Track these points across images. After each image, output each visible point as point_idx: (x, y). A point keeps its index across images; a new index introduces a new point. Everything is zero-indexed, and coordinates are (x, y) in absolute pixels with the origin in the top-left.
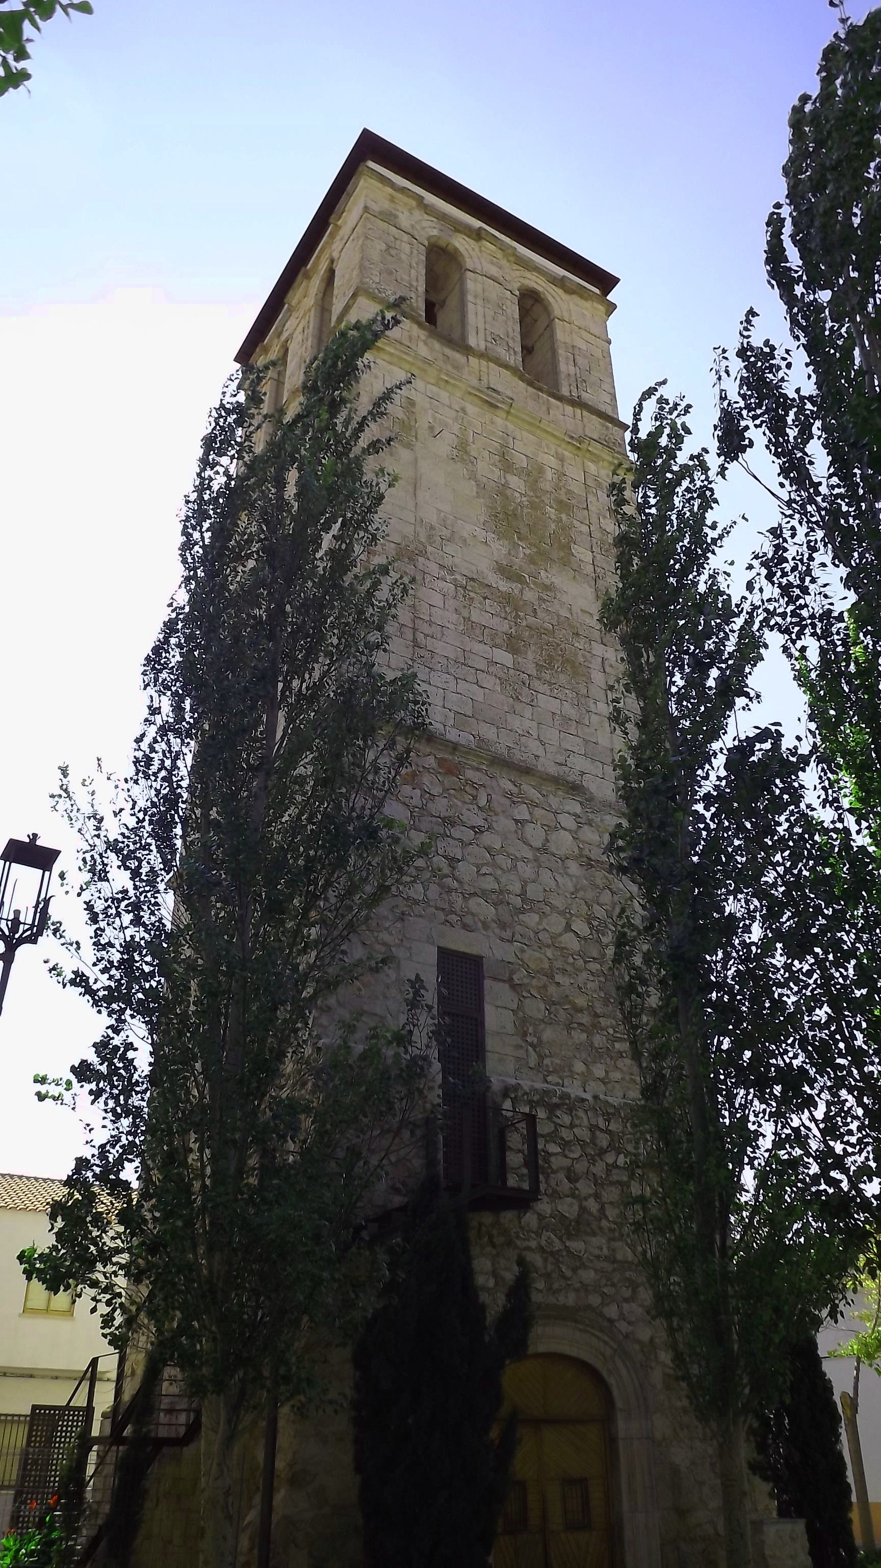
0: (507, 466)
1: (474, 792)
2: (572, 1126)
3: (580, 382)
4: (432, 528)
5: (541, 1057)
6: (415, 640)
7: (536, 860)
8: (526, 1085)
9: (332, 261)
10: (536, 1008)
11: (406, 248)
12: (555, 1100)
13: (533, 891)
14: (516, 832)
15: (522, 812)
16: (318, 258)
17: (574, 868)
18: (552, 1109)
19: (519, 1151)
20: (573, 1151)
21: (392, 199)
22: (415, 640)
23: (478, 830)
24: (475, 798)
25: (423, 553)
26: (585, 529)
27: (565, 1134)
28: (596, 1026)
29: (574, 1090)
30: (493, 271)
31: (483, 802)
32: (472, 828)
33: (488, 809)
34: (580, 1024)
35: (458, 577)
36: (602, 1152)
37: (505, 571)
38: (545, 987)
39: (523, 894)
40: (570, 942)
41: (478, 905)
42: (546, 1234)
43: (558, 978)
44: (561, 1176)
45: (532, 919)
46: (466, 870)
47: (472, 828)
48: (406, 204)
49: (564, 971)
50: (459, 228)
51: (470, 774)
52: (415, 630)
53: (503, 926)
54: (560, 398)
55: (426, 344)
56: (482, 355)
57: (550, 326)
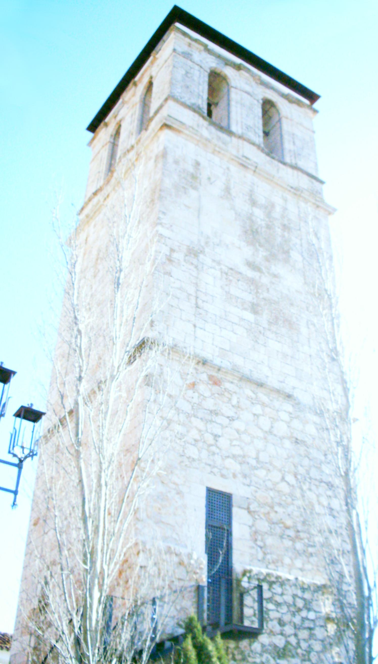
0: (254, 203)
1: (229, 396)
2: (282, 594)
3: (297, 155)
4: (208, 237)
5: (265, 554)
6: (197, 304)
7: (265, 438)
8: (255, 570)
9: (151, 78)
10: (263, 525)
11: (197, 73)
12: (273, 579)
13: (263, 457)
14: (254, 421)
15: (258, 409)
16: (143, 75)
17: (287, 444)
18: (271, 584)
19: (252, 607)
20: (282, 609)
21: (190, 45)
22: (197, 304)
23: (231, 419)
24: (230, 400)
25: (202, 252)
26: (298, 241)
27: (278, 599)
28: (297, 537)
29: (284, 574)
30: (248, 88)
31: (234, 402)
32: (228, 417)
33: (238, 407)
34: (289, 536)
35: (224, 268)
36: (300, 610)
37: (251, 265)
38: (268, 513)
39: (257, 459)
40: (283, 487)
41: (229, 463)
42: (266, 655)
43: (277, 508)
44: (275, 623)
45: (262, 473)
46: (223, 442)
47: (228, 417)
48: (197, 48)
49: (280, 504)
50: (227, 63)
51: (227, 385)
52: (197, 298)
53: (245, 476)
54: (285, 164)
55: (207, 128)
56: (240, 137)
57: (280, 120)
